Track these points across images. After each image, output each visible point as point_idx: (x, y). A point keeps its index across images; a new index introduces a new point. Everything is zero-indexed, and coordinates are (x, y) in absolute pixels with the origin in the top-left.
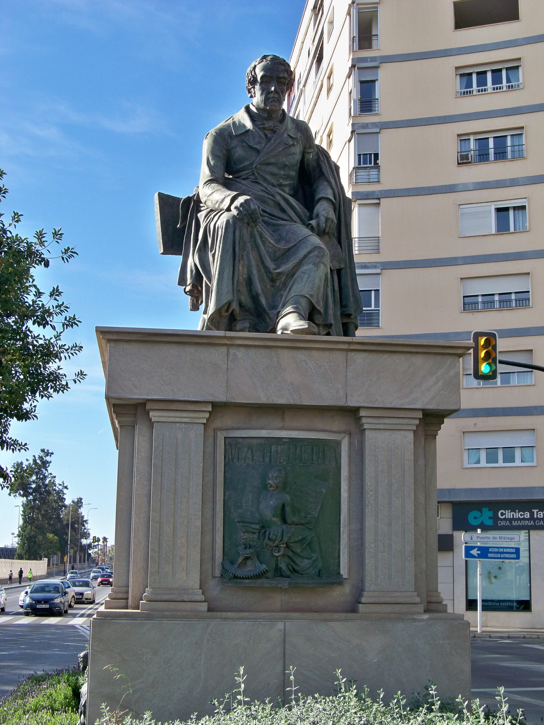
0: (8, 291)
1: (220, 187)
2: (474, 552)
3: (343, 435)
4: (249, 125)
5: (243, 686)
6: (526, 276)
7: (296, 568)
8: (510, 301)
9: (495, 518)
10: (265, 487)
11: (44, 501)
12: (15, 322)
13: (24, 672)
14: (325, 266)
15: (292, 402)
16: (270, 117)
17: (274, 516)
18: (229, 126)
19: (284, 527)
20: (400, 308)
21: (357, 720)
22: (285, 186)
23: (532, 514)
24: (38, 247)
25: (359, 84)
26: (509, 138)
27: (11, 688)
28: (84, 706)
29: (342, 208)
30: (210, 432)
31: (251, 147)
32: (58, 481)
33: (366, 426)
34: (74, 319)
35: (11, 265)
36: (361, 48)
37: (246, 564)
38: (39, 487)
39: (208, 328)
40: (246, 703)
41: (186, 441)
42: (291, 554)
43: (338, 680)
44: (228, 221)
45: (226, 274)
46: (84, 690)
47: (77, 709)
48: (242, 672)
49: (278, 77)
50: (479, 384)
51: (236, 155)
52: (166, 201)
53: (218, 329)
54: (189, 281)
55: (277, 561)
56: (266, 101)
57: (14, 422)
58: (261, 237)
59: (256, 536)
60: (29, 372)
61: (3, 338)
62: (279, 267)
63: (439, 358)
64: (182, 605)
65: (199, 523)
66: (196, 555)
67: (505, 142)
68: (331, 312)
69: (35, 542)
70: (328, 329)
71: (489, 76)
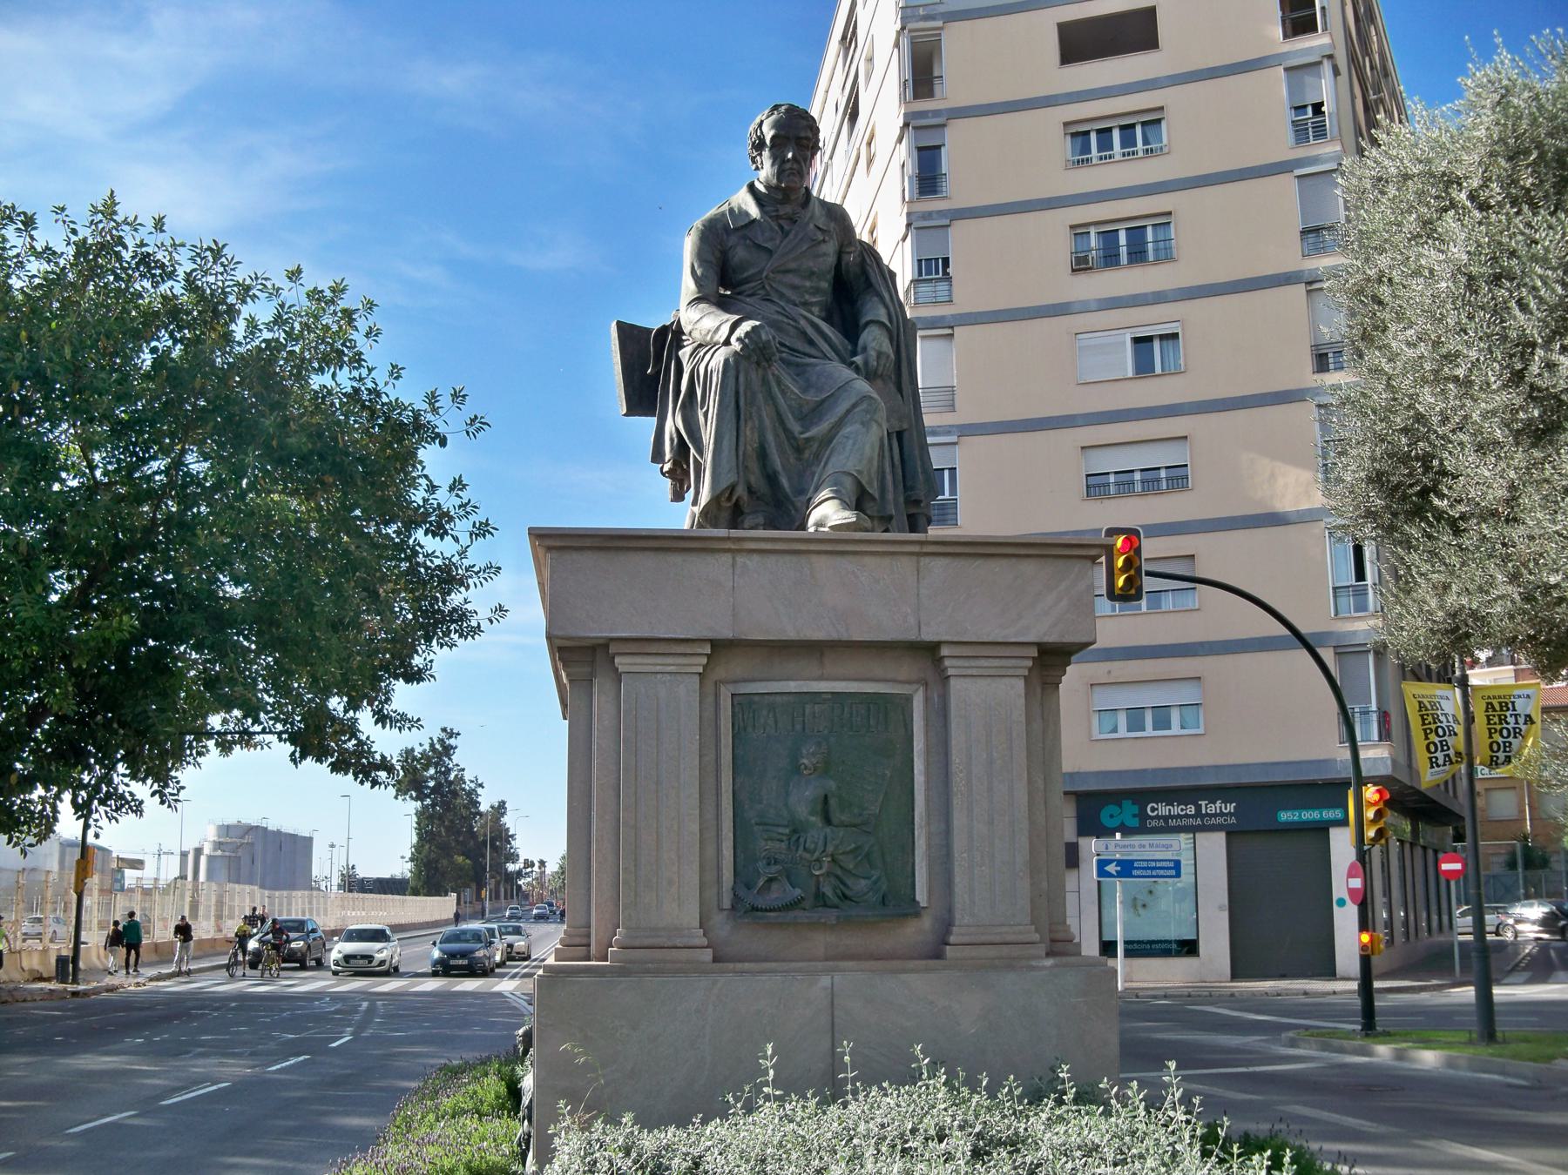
0: (384, 486)
1: (713, 309)
2: (1111, 868)
3: (915, 686)
4: (754, 211)
5: (771, 1072)
6: (1182, 442)
7: (847, 892)
8: (1158, 480)
9: (1143, 816)
10: (796, 769)
11: (447, 807)
12: (398, 533)
13: (432, 1061)
14: (880, 425)
15: (835, 636)
16: (789, 196)
17: (812, 813)
18: (723, 214)
19: (828, 830)
20: (991, 492)
21: (949, 1120)
22: (812, 304)
23: (1198, 808)
24: (430, 417)
25: (915, 153)
26: (1149, 229)
27: (414, 1085)
28: (530, 1107)
29: (902, 334)
30: (710, 688)
31: (759, 247)
32: (468, 776)
33: (950, 672)
34: (487, 524)
35: (390, 445)
36: (916, 96)
37: (769, 889)
38: (439, 786)
39: (700, 526)
40: (777, 1098)
41: (672, 698)
42: (839, 872)
43: (917, 1060)
44: (726, 361)
45: (725, 443)
46: (528, 1083)
47: (516, 1114)
48: (769, 1052)
49: (796, 137)
50: (1114, 609)
51: (736, 259)
52: (628, 333)
53: (715, 526)
54: (668, 456)
55: (818, 883)
56: (780, 174)
57: (399, 686)
58: (779, 383)
59: (784, 845)
60: (420, 609)
61: (380, 557)
62: (806, 429)
63: (1060, 563)
64: (675, 953)
65: (696, 827)
66: (692, 877)
67: (1144, 235)
68: (890, 496)
69: (436, 869)
70: (886, 522)
71: (1116, 134)
